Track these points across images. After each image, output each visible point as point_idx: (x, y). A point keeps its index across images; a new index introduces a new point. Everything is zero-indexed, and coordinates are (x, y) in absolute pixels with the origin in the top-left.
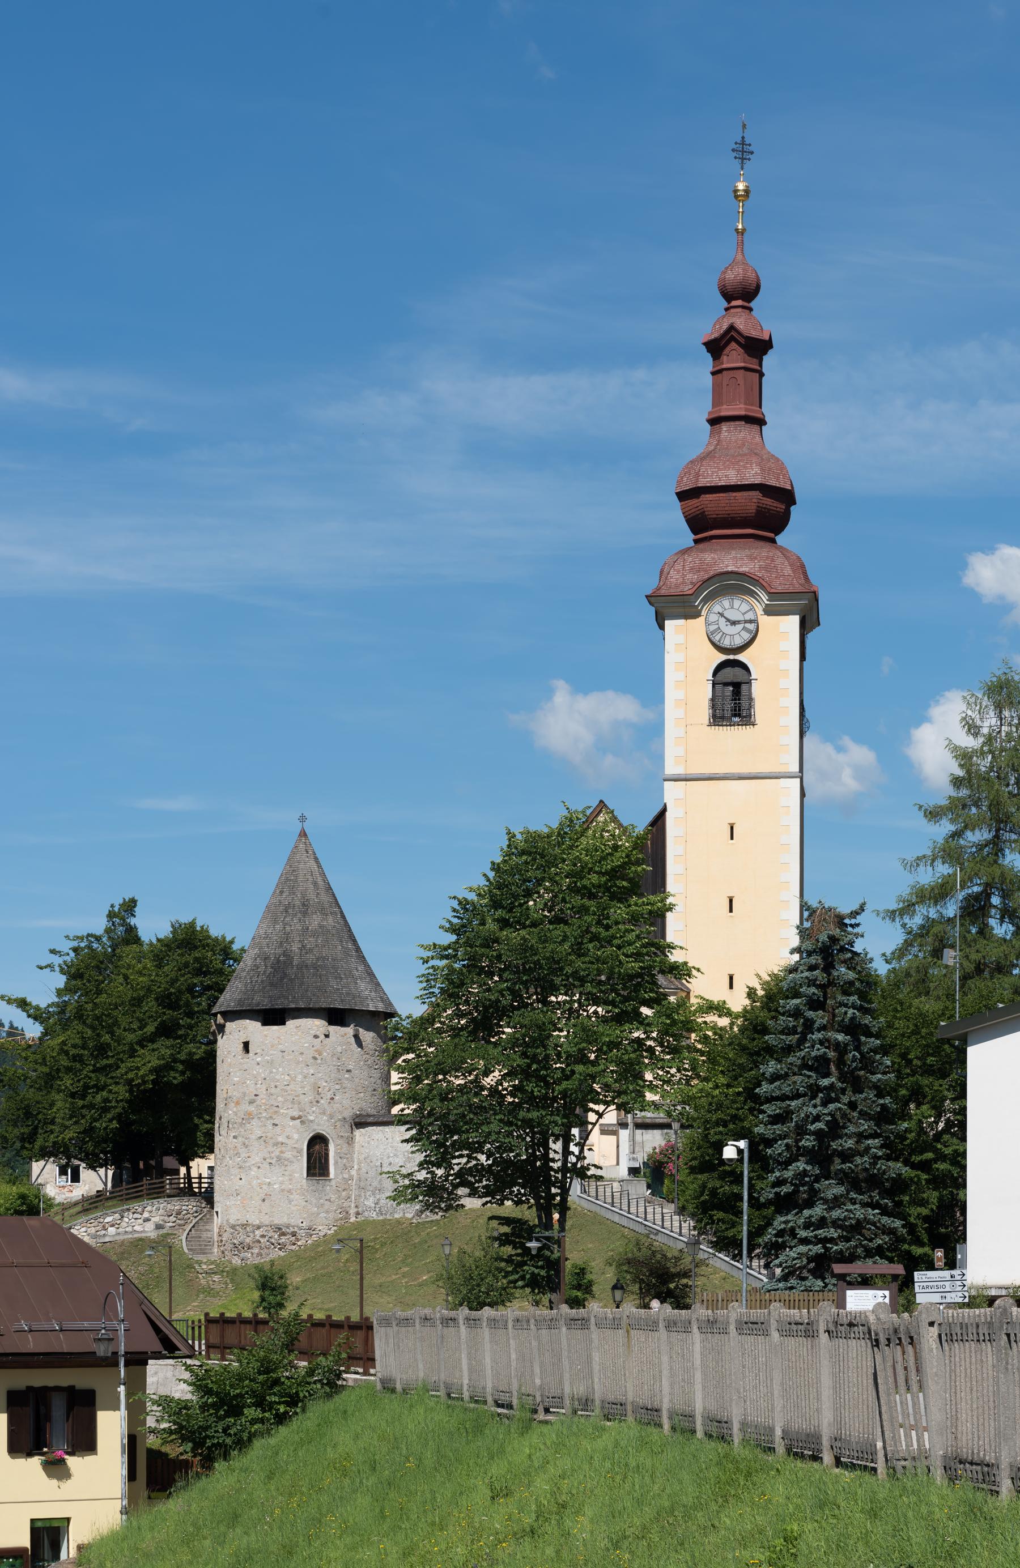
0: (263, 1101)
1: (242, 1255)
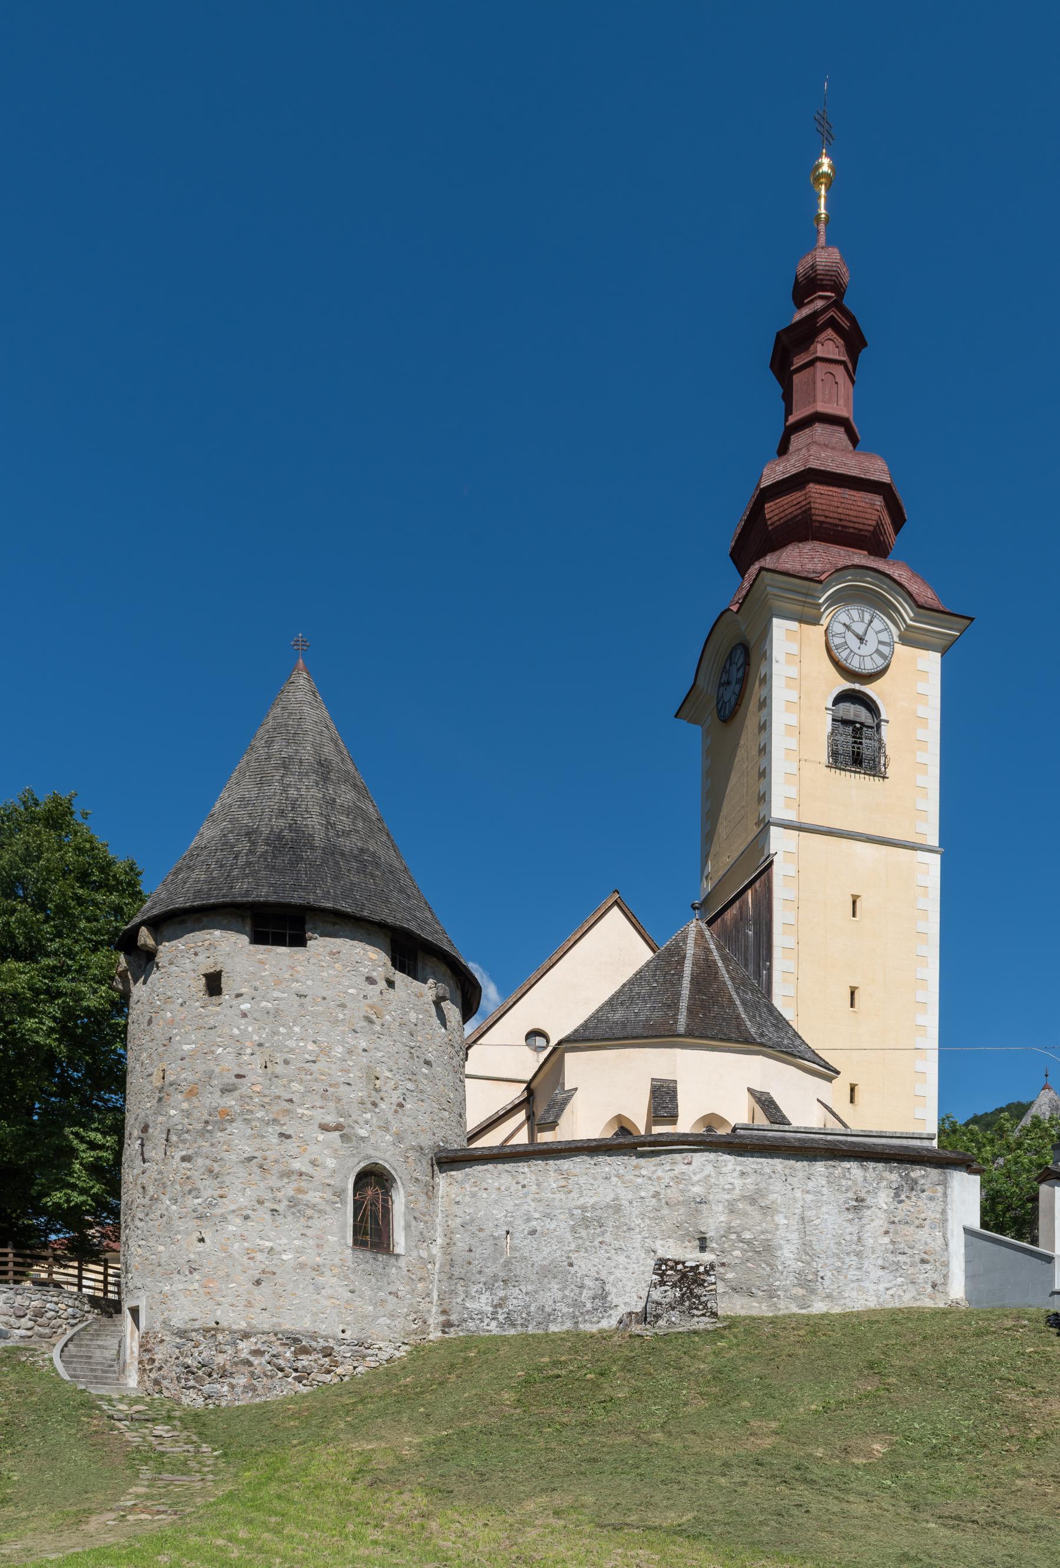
0: (258, 1088)
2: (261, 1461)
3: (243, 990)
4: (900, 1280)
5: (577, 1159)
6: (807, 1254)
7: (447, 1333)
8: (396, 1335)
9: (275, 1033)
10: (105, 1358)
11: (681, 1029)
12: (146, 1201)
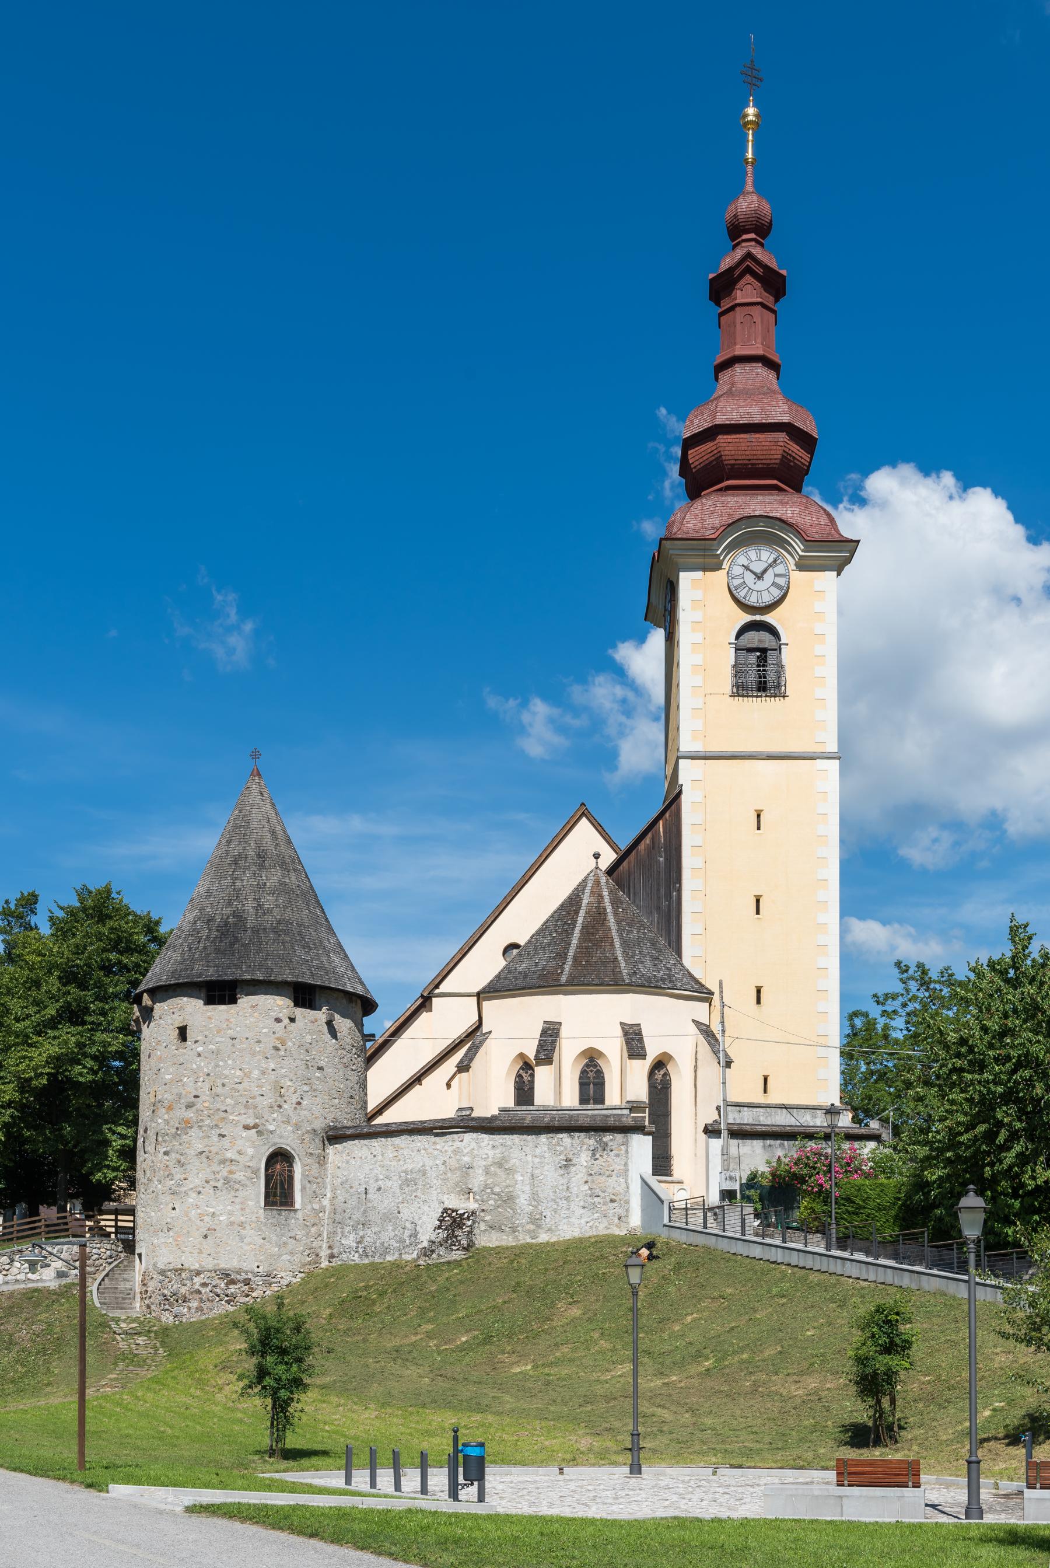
0: (206, 1104)
1: (175, 1310)
3: (199, 1038)
4: (596, 1215)
5: (403, 1137)
6: (535, 1200)
8: (294, 1267)
9: (217, 1066)
11: (564, 979)
12: (145, 1181)
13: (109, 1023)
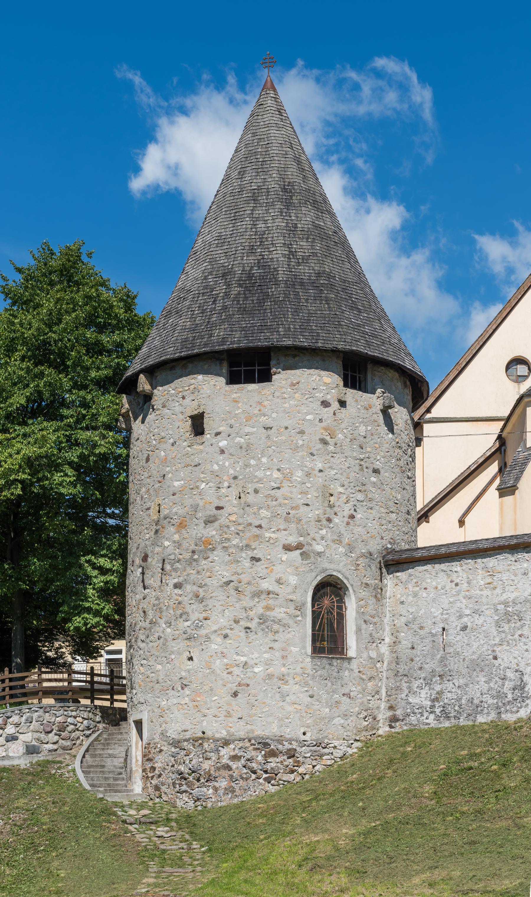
0: (233, 518)
2: (236, 854)
3: (221, 429)
5: (500, 557)
7: (393, 727)
8: (349, 733)
9: (247, 466)
10: (114, 766)
12: (147, 624)
13: (94, 417)
